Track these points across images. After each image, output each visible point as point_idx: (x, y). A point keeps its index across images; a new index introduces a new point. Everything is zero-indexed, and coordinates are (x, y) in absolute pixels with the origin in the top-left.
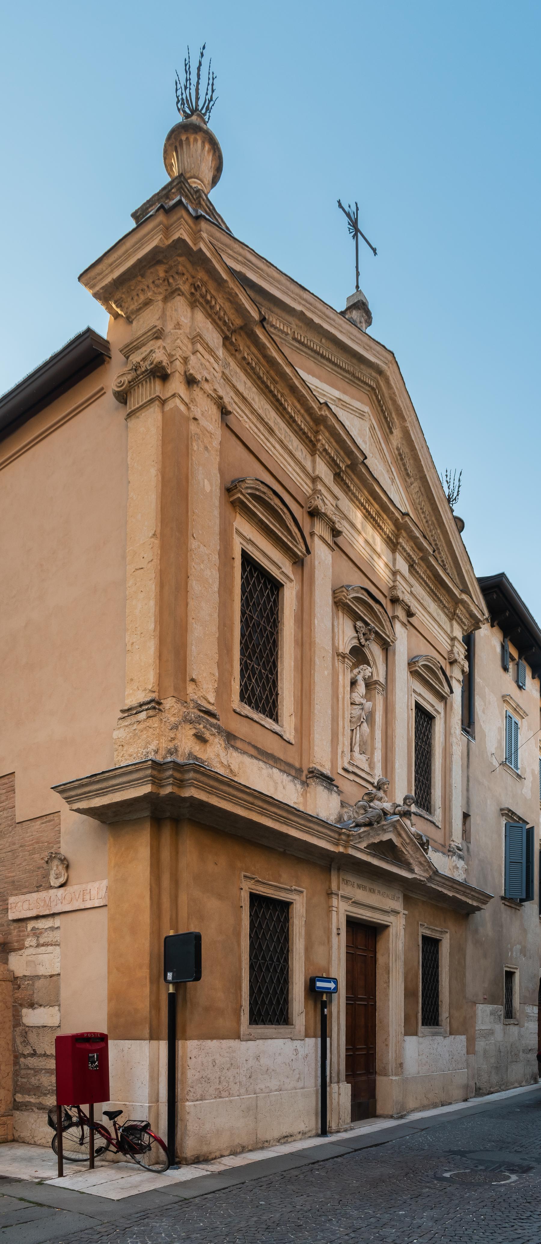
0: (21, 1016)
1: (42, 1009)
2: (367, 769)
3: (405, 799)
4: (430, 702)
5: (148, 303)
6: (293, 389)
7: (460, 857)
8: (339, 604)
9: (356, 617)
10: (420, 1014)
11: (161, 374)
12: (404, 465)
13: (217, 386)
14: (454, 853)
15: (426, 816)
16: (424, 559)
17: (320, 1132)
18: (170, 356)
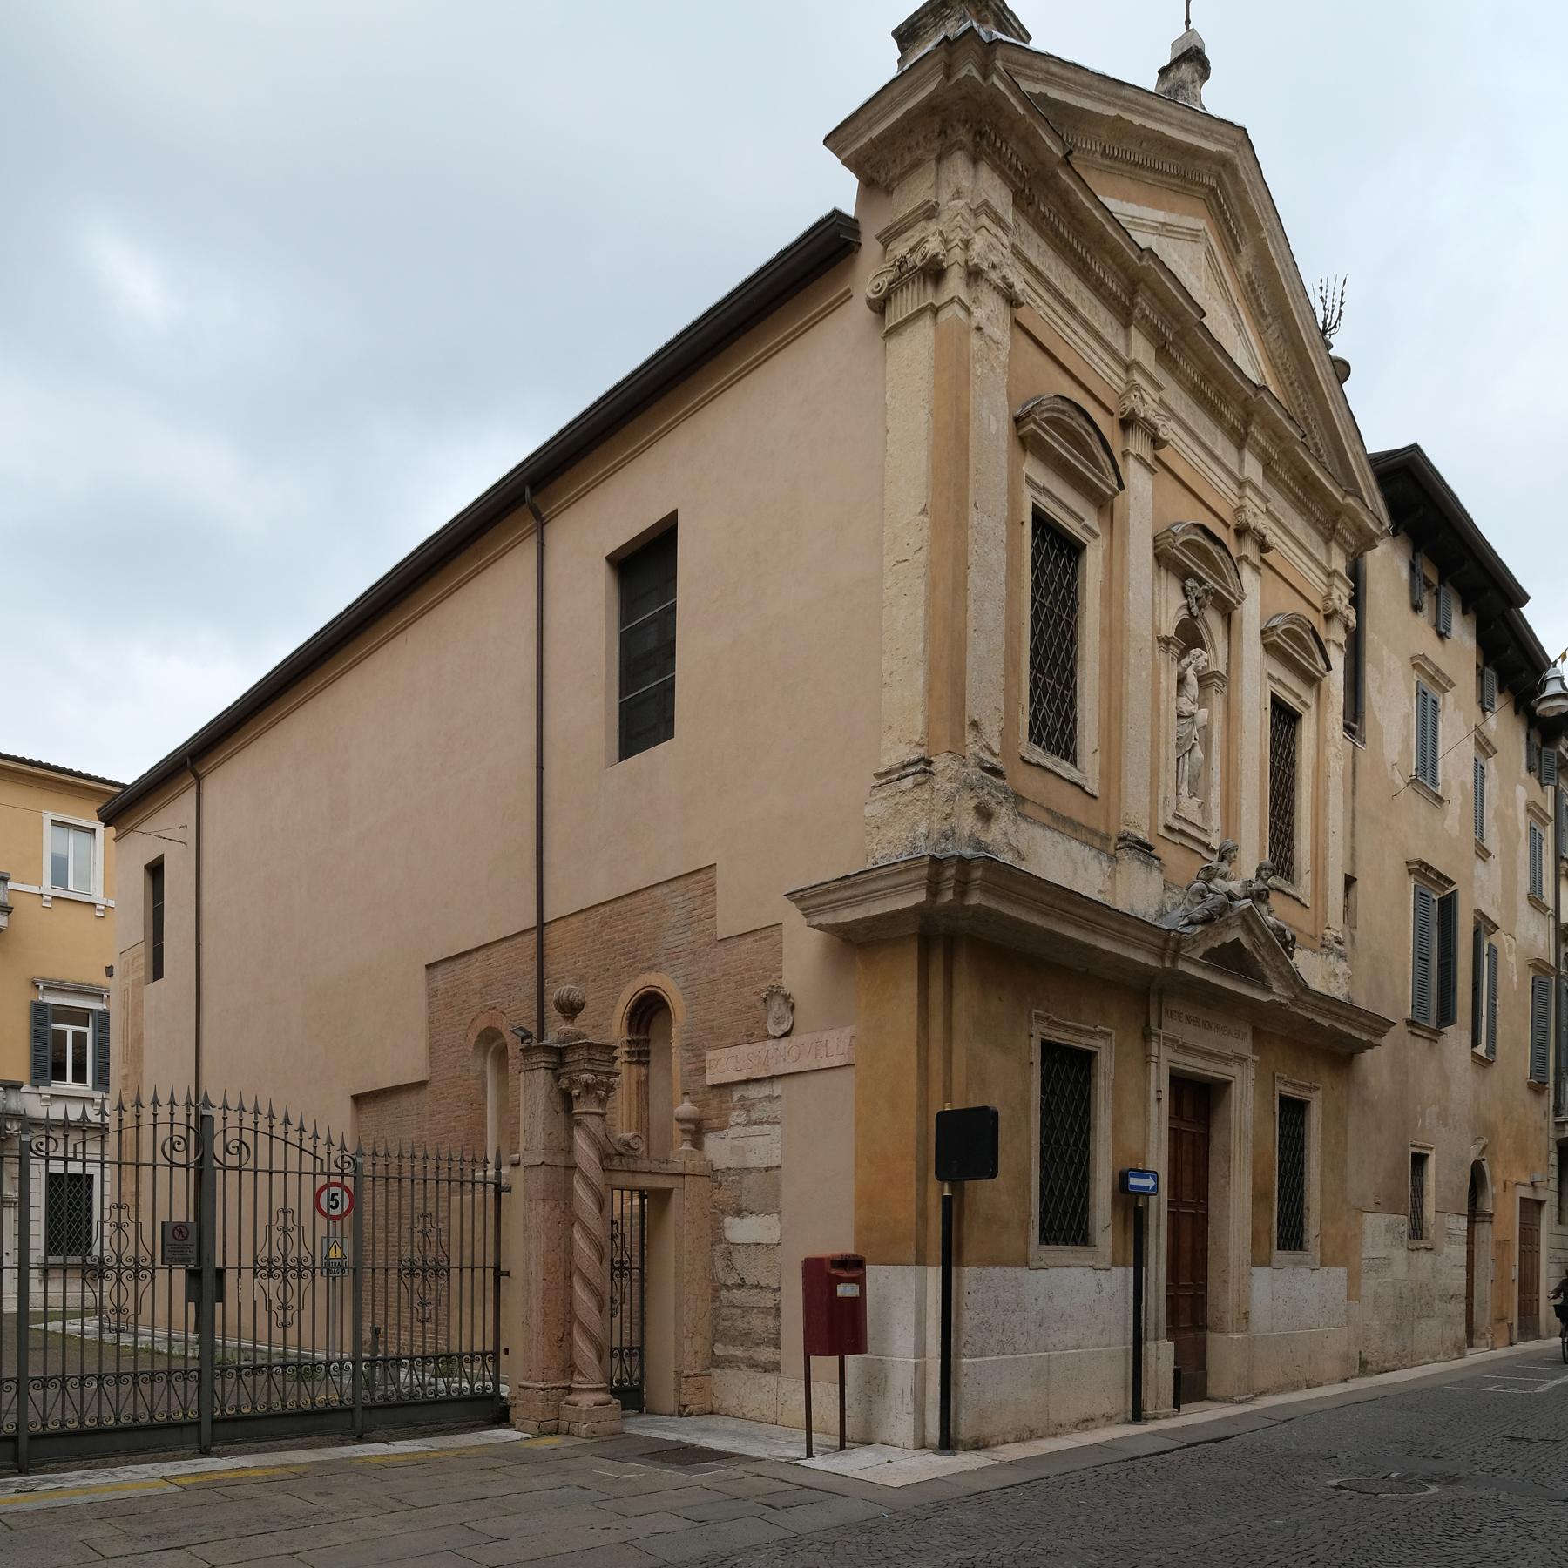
0: (723, 1229)
3: (1259, 870)
4: (1294, 692)
5: (917, 164)
7: (1341, 956)
8: (1163, 559)
9: (1184, 574)
11: (934, 273)
13: (1006, 272)
15: (1287, 890)
17: (1130, 1417)
18: (946, 242)
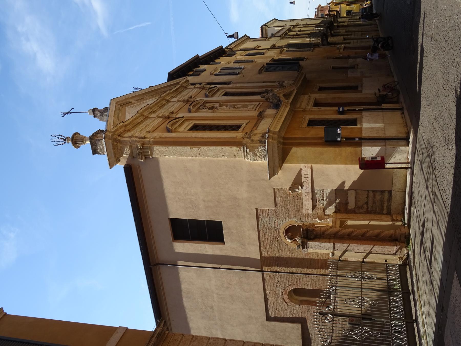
0: (351, 209)
1: (349, 199)
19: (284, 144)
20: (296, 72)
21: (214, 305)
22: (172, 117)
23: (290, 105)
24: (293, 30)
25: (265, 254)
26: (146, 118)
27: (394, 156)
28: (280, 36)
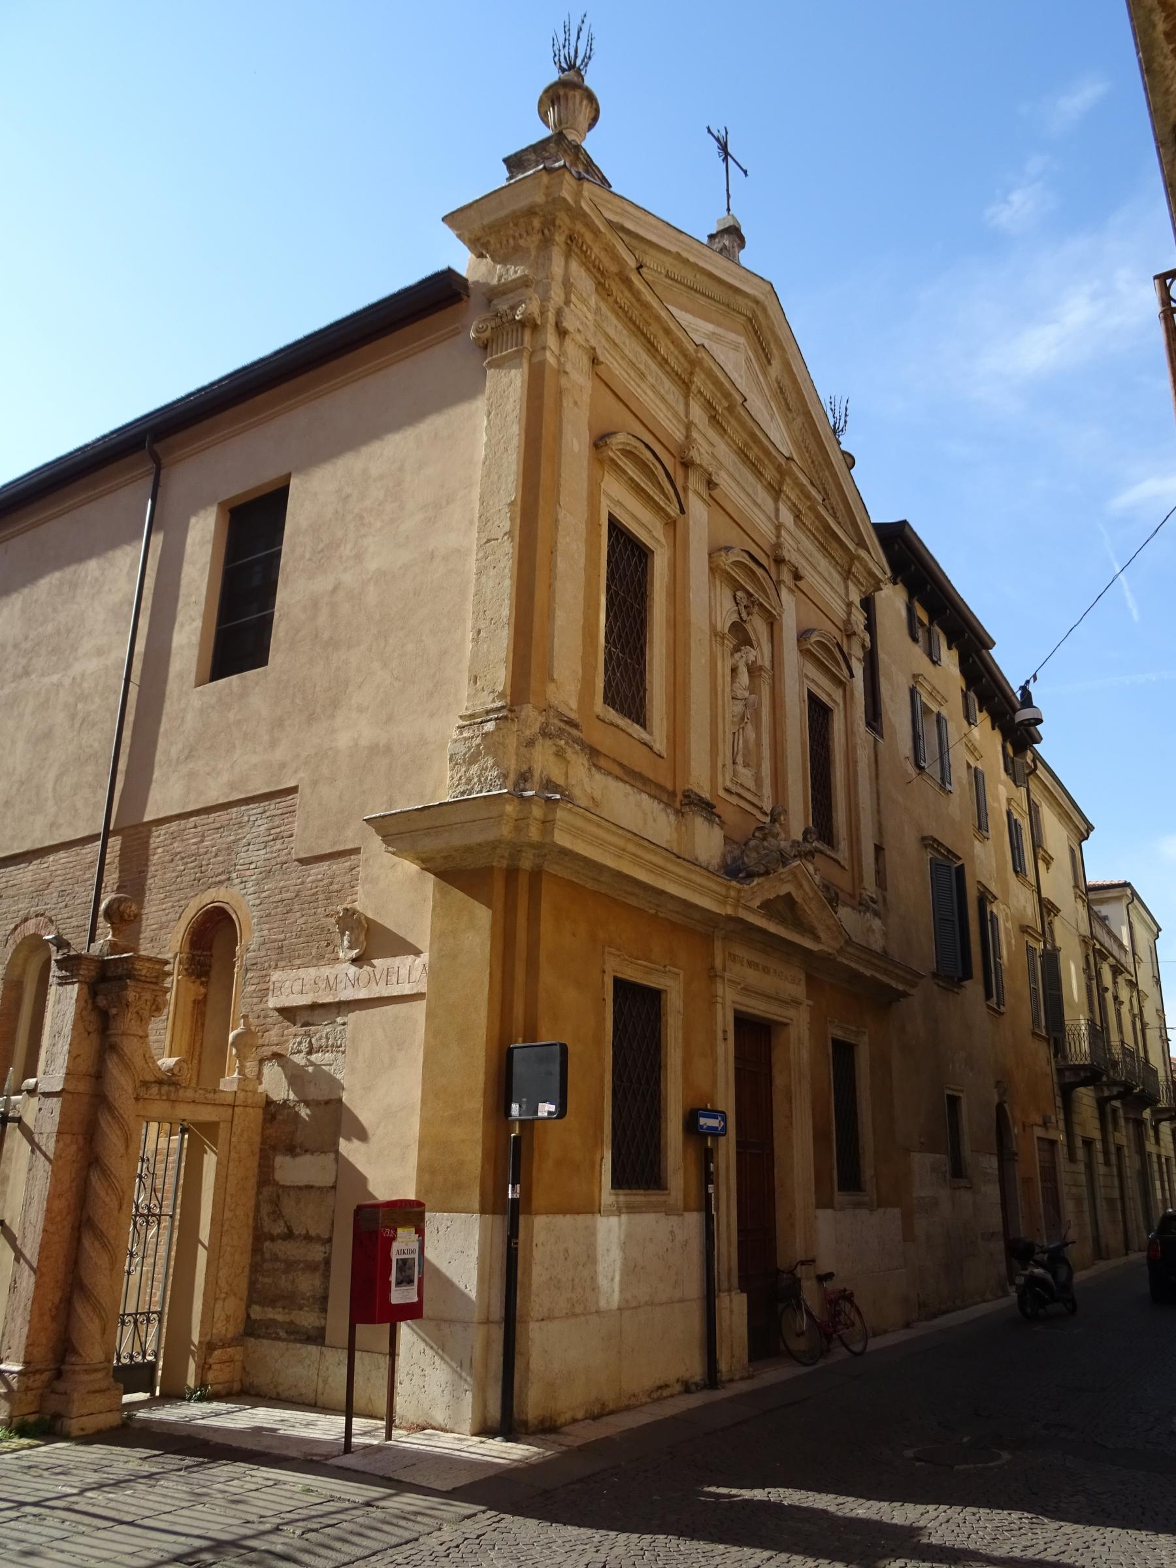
1: (307, 1158)
2: (753, 788)
6: (667, 332)
7: (876, 914)
10: (835, 1172)
12: (785, 400)
14: (868, 908)
15: (829, 853)
16: (813, 509)
19: (512, 874)
20: (933, 966)
21: (33, 676)
22: (850, 647)
23: (729, 918)
24: (1120, 979)
25: (158, 837)
26: (685, 385)
27: (437, 1360)
28: (1093, 937)
